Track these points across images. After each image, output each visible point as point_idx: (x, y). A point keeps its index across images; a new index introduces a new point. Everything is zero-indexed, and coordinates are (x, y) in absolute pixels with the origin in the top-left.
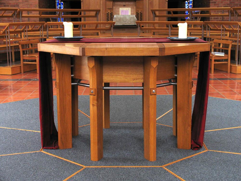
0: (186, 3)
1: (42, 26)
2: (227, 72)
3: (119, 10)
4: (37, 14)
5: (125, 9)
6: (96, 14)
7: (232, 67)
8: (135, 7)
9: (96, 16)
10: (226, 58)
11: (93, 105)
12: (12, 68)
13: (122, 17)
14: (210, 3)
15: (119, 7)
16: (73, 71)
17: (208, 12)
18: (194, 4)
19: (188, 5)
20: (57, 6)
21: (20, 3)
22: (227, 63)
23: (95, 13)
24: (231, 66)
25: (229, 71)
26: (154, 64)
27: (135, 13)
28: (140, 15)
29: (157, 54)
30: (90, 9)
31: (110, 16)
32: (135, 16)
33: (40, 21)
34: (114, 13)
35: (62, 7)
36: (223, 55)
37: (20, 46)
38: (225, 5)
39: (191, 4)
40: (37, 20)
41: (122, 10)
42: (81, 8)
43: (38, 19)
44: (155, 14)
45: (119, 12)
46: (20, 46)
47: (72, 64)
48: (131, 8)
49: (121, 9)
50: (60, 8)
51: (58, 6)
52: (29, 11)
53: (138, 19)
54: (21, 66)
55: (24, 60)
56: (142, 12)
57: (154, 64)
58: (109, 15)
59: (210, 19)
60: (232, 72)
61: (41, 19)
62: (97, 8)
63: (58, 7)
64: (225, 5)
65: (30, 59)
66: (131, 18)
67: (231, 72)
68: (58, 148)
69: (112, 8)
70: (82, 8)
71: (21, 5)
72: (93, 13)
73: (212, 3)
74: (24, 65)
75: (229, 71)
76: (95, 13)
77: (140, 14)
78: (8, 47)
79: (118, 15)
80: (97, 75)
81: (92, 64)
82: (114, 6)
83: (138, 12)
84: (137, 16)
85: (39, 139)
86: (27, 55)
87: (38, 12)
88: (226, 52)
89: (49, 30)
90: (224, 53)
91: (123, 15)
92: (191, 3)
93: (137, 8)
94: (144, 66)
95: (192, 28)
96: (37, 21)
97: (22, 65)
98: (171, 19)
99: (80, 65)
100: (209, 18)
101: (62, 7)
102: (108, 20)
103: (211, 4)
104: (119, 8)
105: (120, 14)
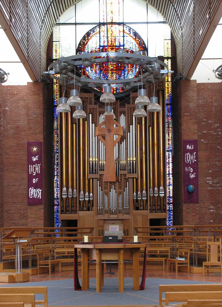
0: (167, 221)
1: (51, 240)
2: (188, 272)
3: (109, 227)
4: (41, 231)
5: (114, 226)
6: (91, 231)
7: (191, 269)
8: (122, 225)
9: (91, 232)
10: (186, 262)
11: (98, 269)
12: (32, 270)
13: (111, 233)
14: (183, 221)
15: (109, 225)
16: (88, 256)
17: (182, 229)
18: (174, 221)
19: (169, 223)
20: (55, 224)
21: (29, 223)
22: (188, 266)
23: (90, 230)
24: (190, 268)
25: (189, 272)
26: (122, 252)
27: (122, 229)
28: (126, 231)
29: (123, 247)
30: (85, 227)
31: (101, 232)
32: (122, 232)
33: (44, 237)
34: (105, 230)
35: (60, 225)
36: (184, 260)
37: (38, 255)
38: (195, 223)
39: (172, 222)
40: (42, 236)
41: (111, 227)
42: (77, 227)
43: (43, 235)
44: (137, 230)
45: (109, 229)
46: (38, 255)
47: (88, 253)
48: (119, 225)
49: (111, 226)
50: (58, 226)
51: (56, 224)
52: (38, 229)
53: (125, 235)
54: (37, 269)
55: (40, 265)
56: (128, 229)
57: (122, 252)
58: (101, 231)
59: (184, 234)
60: (191, 272)
61: (45, 235)
62: (91, 226)
63: (56, 225)
64: (195, 223)
65: (44, 264)
66: (119, 233)
67: (190, 273)
68: (81, 290)
69: (103, 225)
70: (78, 226)
71: (29, 224)
72: (89, 230)
73: (185, 221)
74: (40, 268)
75: (189, 272)
76: (90, 230)
77: (126, 230)
78: (30, 255)
79: (108, 231)
80: (99, 256)
81: (98, 252)
82: (105, 224)
83: (125, 229)
84: (124, 232)
85: (74, 289)
86: (41, 261)
87: (43, 230)
88: (186, 258)
89: (57, 243)
90: (184, 259)
91: (113, 232)
92: (172, 221)
93: (124, 226)
94: (118, 254)
95: (168, 241)
96: (42, 237)
97: (38, 268)
98: (154, 234)
99: (92, 253)
100: (183, 234)
101: (60, 225)
102: (100, 235)
103: (184, 222)
104: (109, 226)
105: (110, 231)
